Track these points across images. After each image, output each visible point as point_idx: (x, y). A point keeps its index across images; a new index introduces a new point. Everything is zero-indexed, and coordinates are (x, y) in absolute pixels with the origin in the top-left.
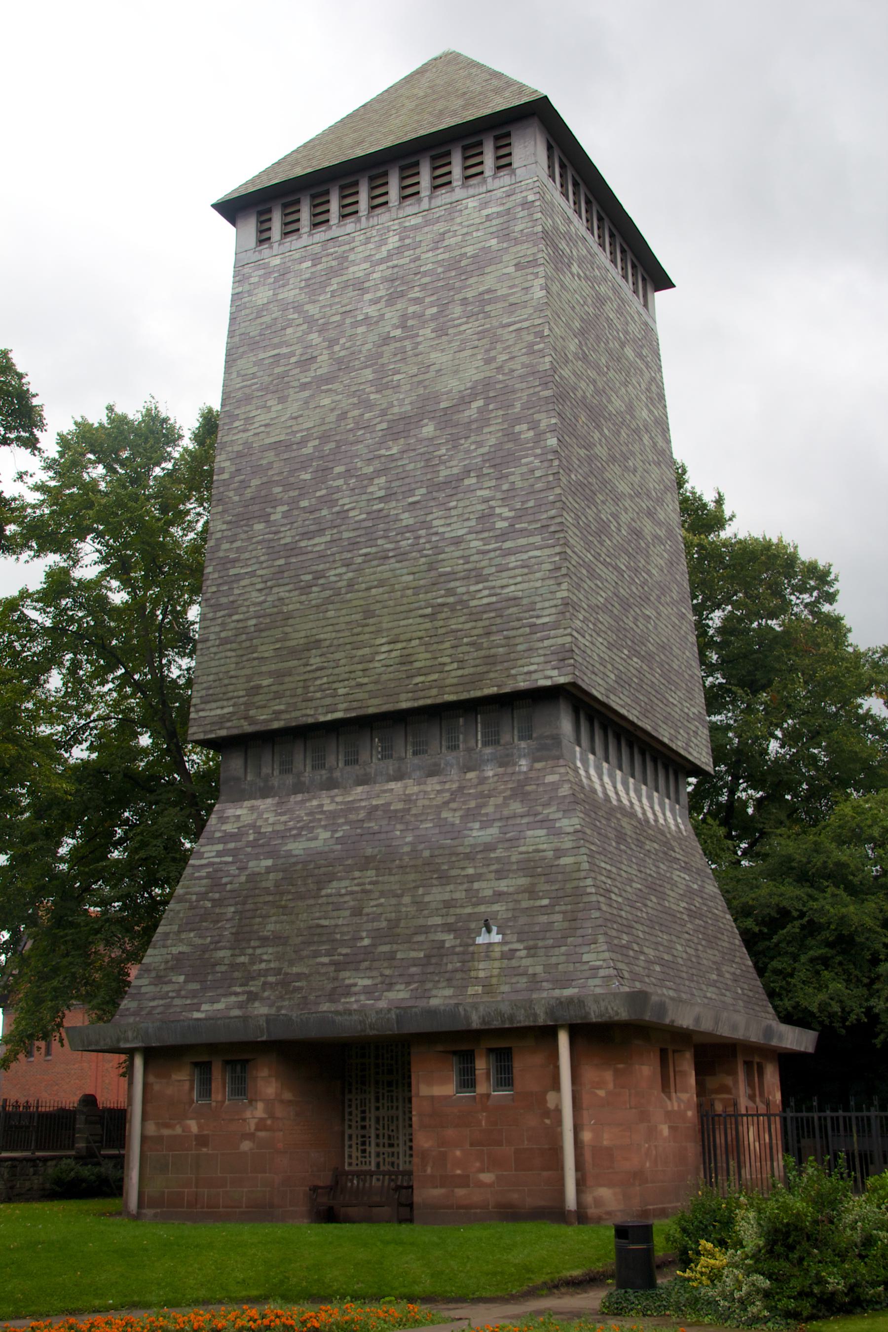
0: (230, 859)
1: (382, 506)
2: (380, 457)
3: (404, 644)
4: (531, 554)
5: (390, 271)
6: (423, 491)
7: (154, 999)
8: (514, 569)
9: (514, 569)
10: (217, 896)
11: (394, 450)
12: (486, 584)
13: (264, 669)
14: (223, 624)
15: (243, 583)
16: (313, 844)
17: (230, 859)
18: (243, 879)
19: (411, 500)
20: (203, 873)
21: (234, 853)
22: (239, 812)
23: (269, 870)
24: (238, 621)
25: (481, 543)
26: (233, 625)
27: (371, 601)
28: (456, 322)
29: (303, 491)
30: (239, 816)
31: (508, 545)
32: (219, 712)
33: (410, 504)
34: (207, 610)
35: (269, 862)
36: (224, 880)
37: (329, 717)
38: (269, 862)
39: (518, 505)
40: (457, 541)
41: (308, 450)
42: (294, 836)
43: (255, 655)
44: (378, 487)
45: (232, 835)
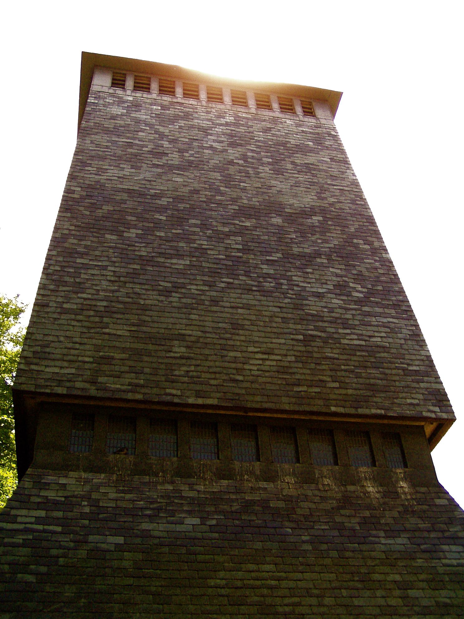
0: (59, 529)
1: (240, 254)
2: (234, 224)
3: (279, 358)
4: (391, 320)
5: (230, 131)
6: (279, 255)
7: (177, 496)
8: (374, 326)
9: (374, 326)
10: (43, 569)
11: (248, 224)
12: (353, 331)
13: (117, 344)
14: (65, 297)
15: (90, 271)
16: (179, 528)
17: (59, 529)
18: (82, 553)
19: (268, 258)
20: (19, 539)
21: (64, 522)
22: (63, 481)
23: (119, 548)
24: (85, 299)
25: (342, 302)
26: (78, 301)
27: (85, 148)
28: (289, 171)
29: (157, 226)
30: (64, 485)
31: (366, 309)
32: (57, 370)
33: (267, 260)
34: (47, 282)
35: (120, 540)
36: (54, 552)
37: (200, 401)
38: (120, 540)
39: (370, 286)
40: (319, 296)
41: (164, 201)
42: (149, 516)
43: (107, 331)
44: (235, 242)
45: (56, 503)
